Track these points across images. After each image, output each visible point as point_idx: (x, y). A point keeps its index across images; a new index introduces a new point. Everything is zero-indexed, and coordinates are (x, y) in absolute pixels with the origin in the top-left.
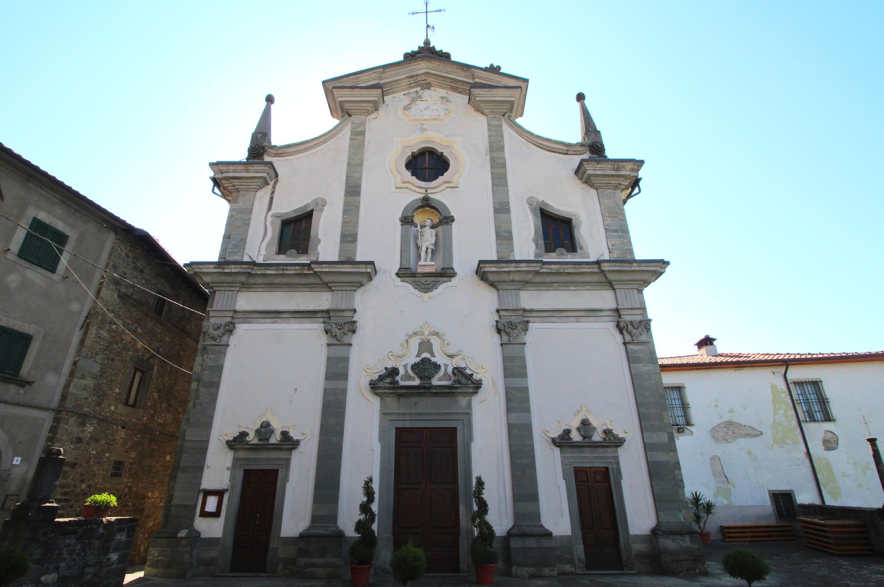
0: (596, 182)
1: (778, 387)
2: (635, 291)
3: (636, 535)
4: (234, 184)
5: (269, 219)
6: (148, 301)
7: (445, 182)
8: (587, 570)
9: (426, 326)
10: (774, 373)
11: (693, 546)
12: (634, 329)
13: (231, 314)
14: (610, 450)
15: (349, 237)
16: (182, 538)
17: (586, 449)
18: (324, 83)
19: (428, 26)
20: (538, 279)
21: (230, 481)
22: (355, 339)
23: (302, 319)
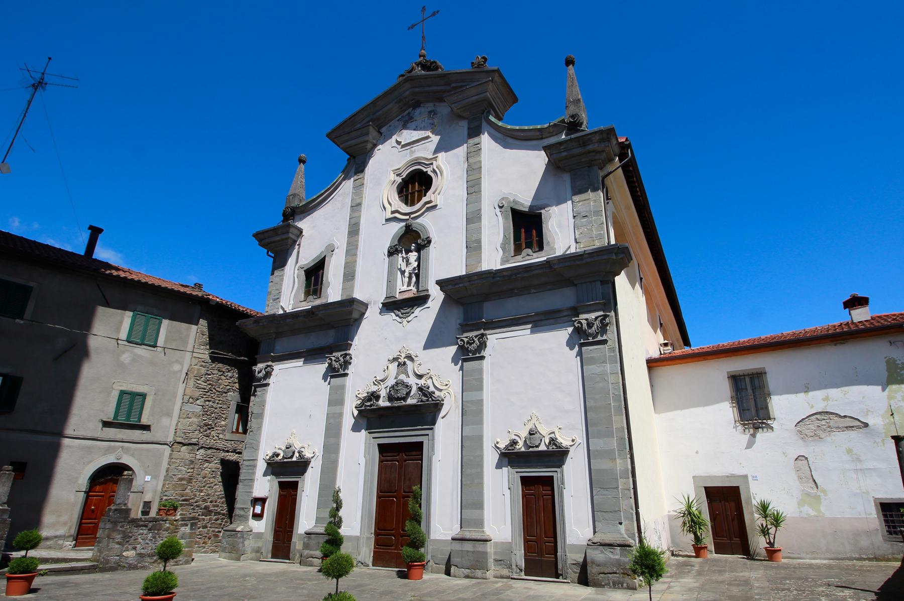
1: (898, 362)
3: (573, 545)
5: (296, 271)
10: (891, 343)
11: (623, 559)
15: (349, 276)
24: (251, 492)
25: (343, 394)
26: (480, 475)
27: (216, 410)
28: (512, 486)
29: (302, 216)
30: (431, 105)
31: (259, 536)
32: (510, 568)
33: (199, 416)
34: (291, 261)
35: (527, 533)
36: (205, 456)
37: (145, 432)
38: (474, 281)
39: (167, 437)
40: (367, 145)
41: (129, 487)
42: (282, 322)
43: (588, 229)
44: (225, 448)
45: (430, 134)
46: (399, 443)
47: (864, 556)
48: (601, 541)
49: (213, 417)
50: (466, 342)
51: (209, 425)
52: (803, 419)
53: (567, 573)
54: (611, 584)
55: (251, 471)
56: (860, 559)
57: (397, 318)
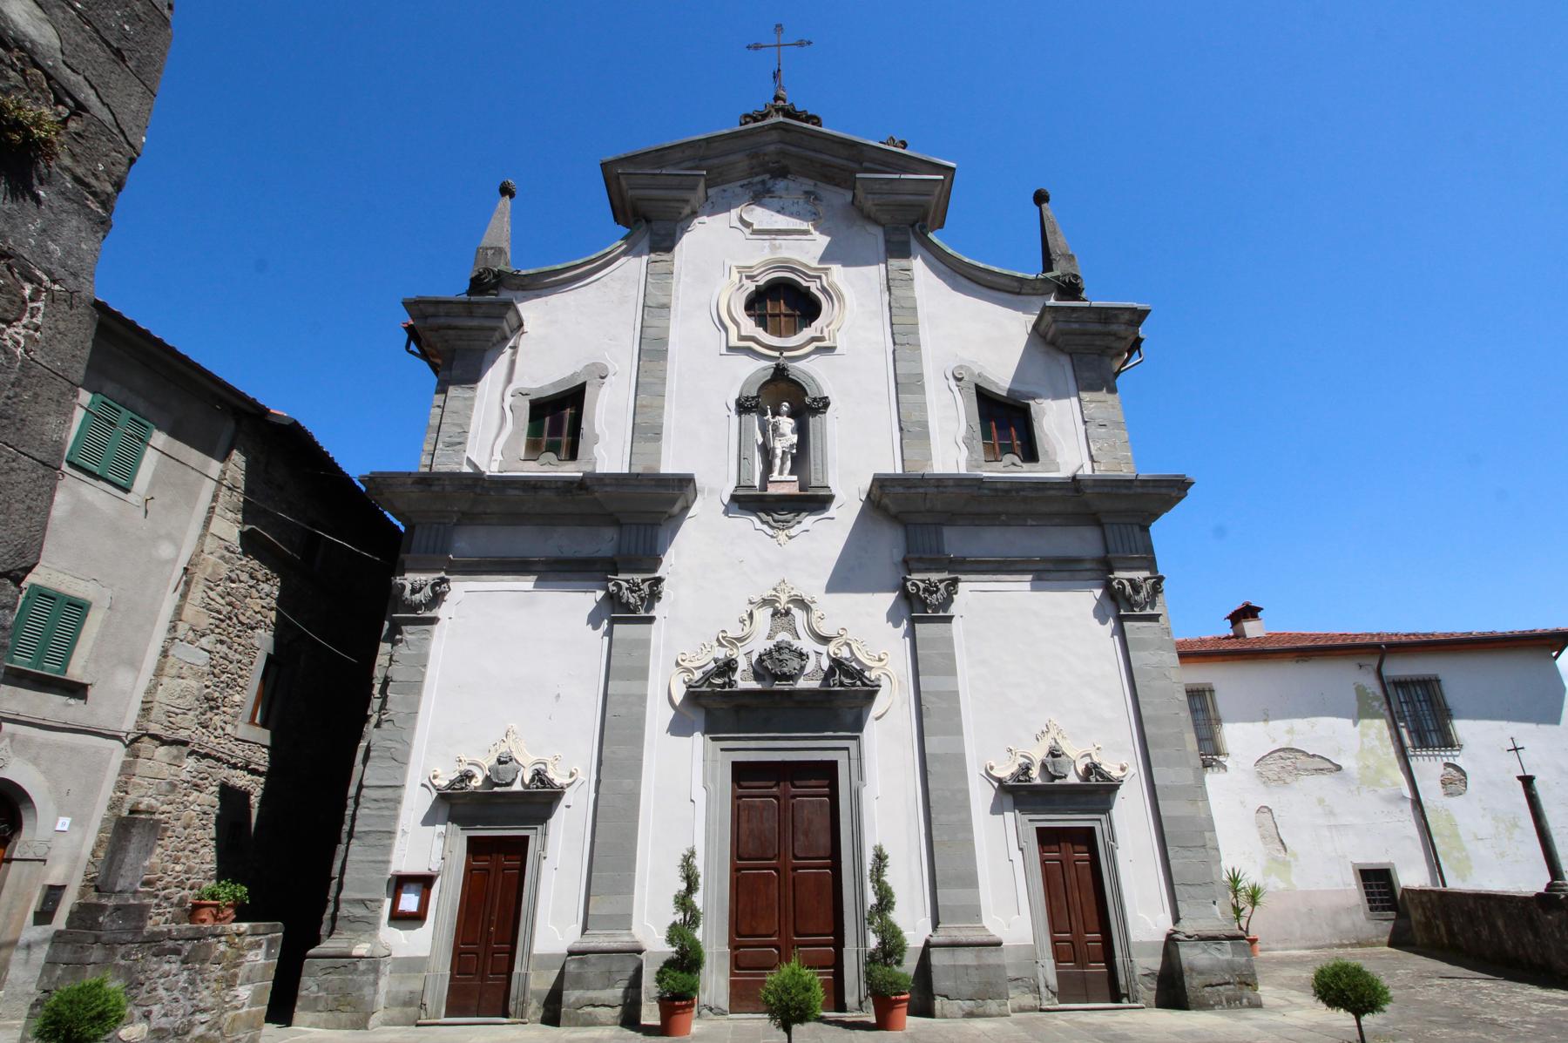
1: (1368, 691)
2: (1137, 529)
5: (508, 400)
8: (1060, 1003)
10: (1360, 666)
11: (1237, 959)
15: (646, 430)
24: (388, 862)
25: (646, 657)
26: (967, 826)
27: (231, 666)
28: (1025, 844)
29: (525, 293)
30: (811, 182)
31: (412, 965)
32: (1035, 992)
33: (202, 676)
34: (494, 376)
35: (462, 940)
36: (195, 774)
37: (72, 701)
38: (945, 487)
39: (121, 719)
40: (683, 208)
41: (150, 845)
42: (492, 493)
43: (1109, 446)
44: (232, 757)
45: (811, 228)
46: (783, 762)
47: (1346, 942)
48: (1199, 933)
49: (222, 682)
50: (921, 589)
51: (213, 700)
52: (1264, 757)
53: (1137, 991)
54: (1225, 1003)
55: (386, 813)
56: (1341, 946)
57: (765, 527)
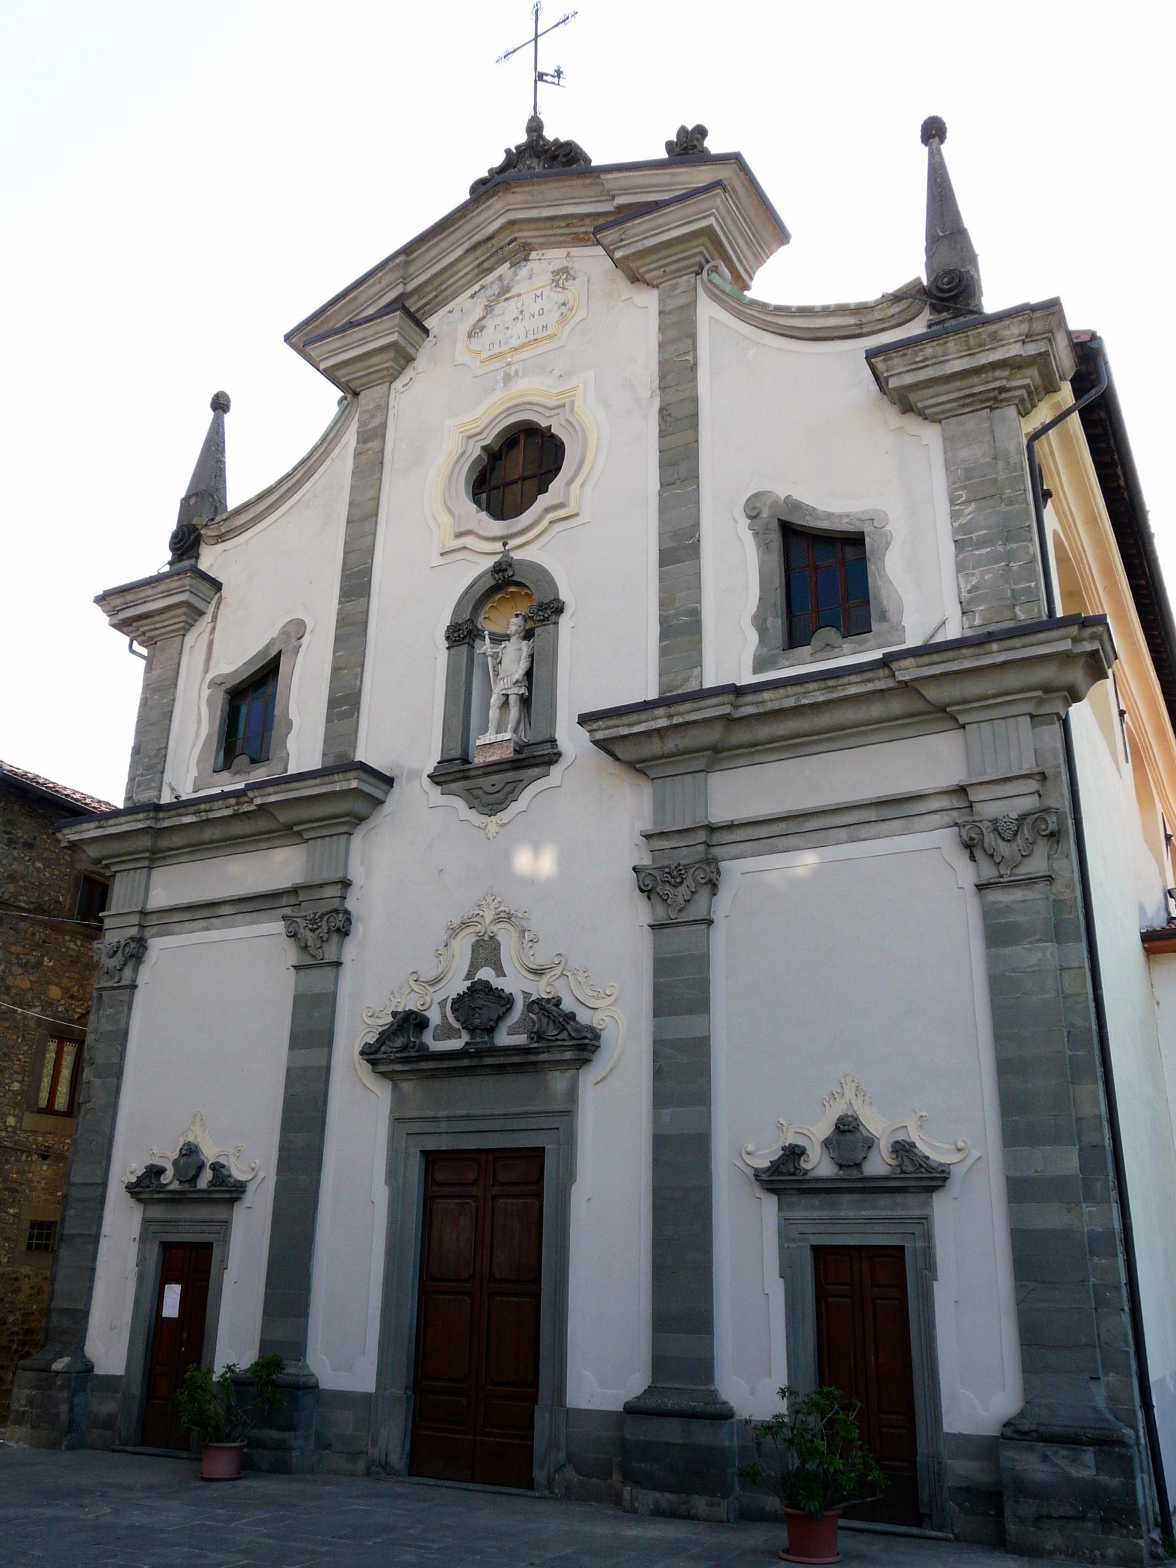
0: (927, 403)
4: (142, 629)
6: (58, 902)
7: (548, 510)
9: (489, 899)
11: (1103, 1479)
12: (1002, 844)
13: (702, 836)
14: (910, 1199)
16: (58, 1373)
17: (846, 1198)
18: (288, 338)
19: (540, 77)
20: (740, 736)
21: (137, 1266)
22: (351, 951)
23: (255, 915)
48: (1042, 1429)
